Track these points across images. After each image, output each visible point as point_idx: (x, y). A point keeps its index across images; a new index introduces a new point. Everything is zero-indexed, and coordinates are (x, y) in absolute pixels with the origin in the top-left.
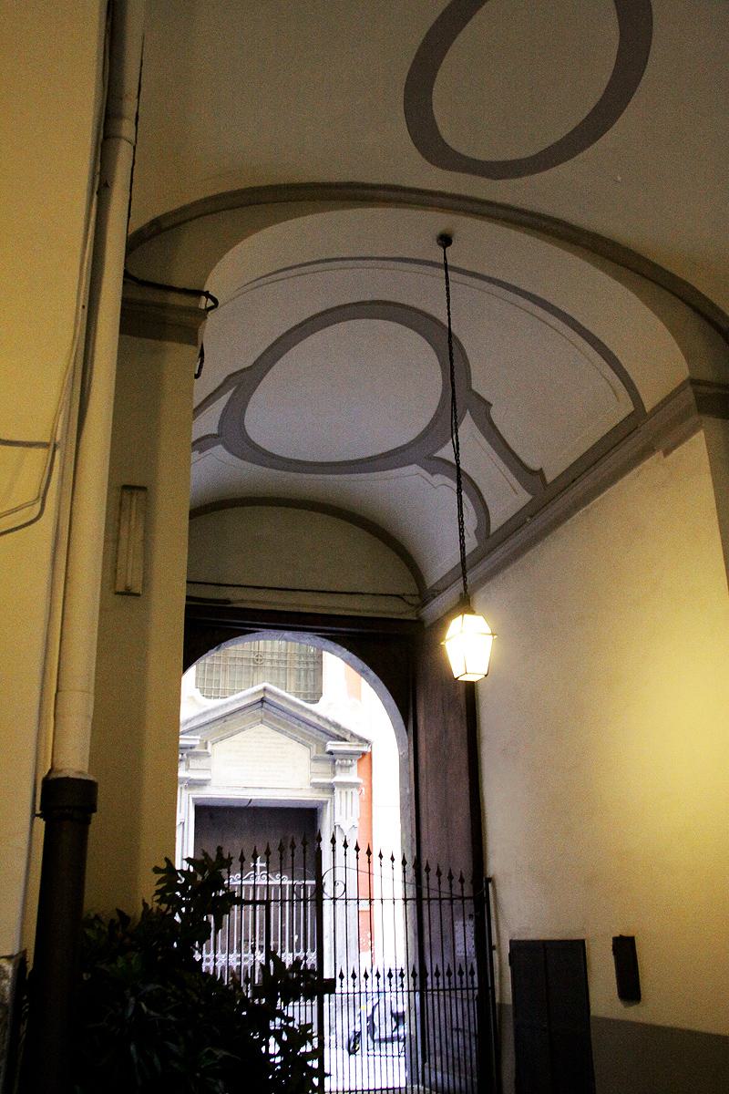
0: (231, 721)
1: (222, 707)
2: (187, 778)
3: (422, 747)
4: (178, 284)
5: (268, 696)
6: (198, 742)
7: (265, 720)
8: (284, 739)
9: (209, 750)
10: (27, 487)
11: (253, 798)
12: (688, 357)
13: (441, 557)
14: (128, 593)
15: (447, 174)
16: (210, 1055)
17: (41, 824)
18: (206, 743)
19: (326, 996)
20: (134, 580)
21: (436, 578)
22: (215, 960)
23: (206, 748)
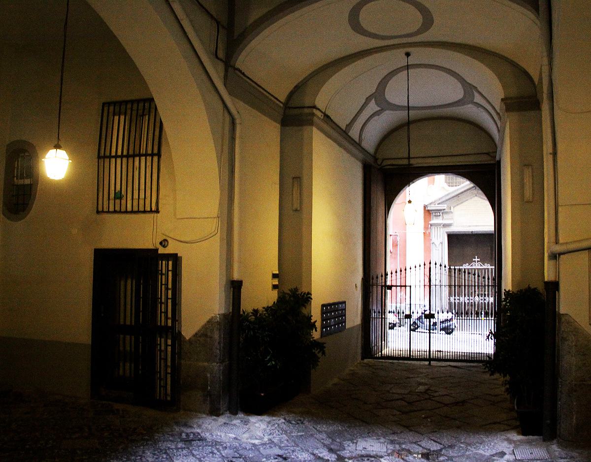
1: (455, 191)
4: (307, 105)
7: (477, 195)
9: (452, 210)
11: (473, 230)
15: (389, 41)
18: (450, 207)
22: (455, 299)
23: (450, 209)
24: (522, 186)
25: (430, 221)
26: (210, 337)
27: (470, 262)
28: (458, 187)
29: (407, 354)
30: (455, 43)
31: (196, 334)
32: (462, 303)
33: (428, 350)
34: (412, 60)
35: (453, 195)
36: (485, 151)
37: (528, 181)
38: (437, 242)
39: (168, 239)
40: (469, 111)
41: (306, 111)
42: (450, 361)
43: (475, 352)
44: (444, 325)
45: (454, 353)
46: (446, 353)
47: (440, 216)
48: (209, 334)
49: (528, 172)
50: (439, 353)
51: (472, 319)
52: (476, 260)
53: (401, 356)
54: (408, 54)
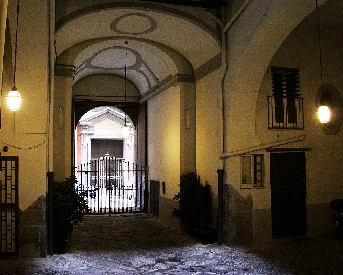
0: (100, 118)
2: (88, 133)
3: (138, 133)
4: (68, 64)
5: (109, 111)
6: (91, 124)
8: (114, 122)
9: (94, 126)
10: (43, 139)
12: (178, 69)
13: (144, 87)
14: (61, 128)
16: (70, 204)
17: (48, 178)
19: (111, 190)
20: (62, 125)
21: (142, 94)
24: (186, 121)
25: (81, 131)
26: (40, 209)
27: (104, 155)
28: (99, 112)
29: (97, 211)
30: (163, 44)
31: (30, 207)
32: (114, 179)
33: (98, 208)
34: (128, 46)
35: (96, 117)
36: (133, 96)
37: (188, 118)
38: (85, 144)
39: (8, 146)
40: (132, 74)
41: (68, 67)
42: (103, 214)
43: (130, 207)
44: (91, 193)
45: (116, 209)
46: (102, 209)
47: (86, 128)
48: (39, 207)
49: (188, 114)
50: (108, 209)
51: (130, 189)
52: (107, 155)
53: (92, 212)
54: (126, 43)
